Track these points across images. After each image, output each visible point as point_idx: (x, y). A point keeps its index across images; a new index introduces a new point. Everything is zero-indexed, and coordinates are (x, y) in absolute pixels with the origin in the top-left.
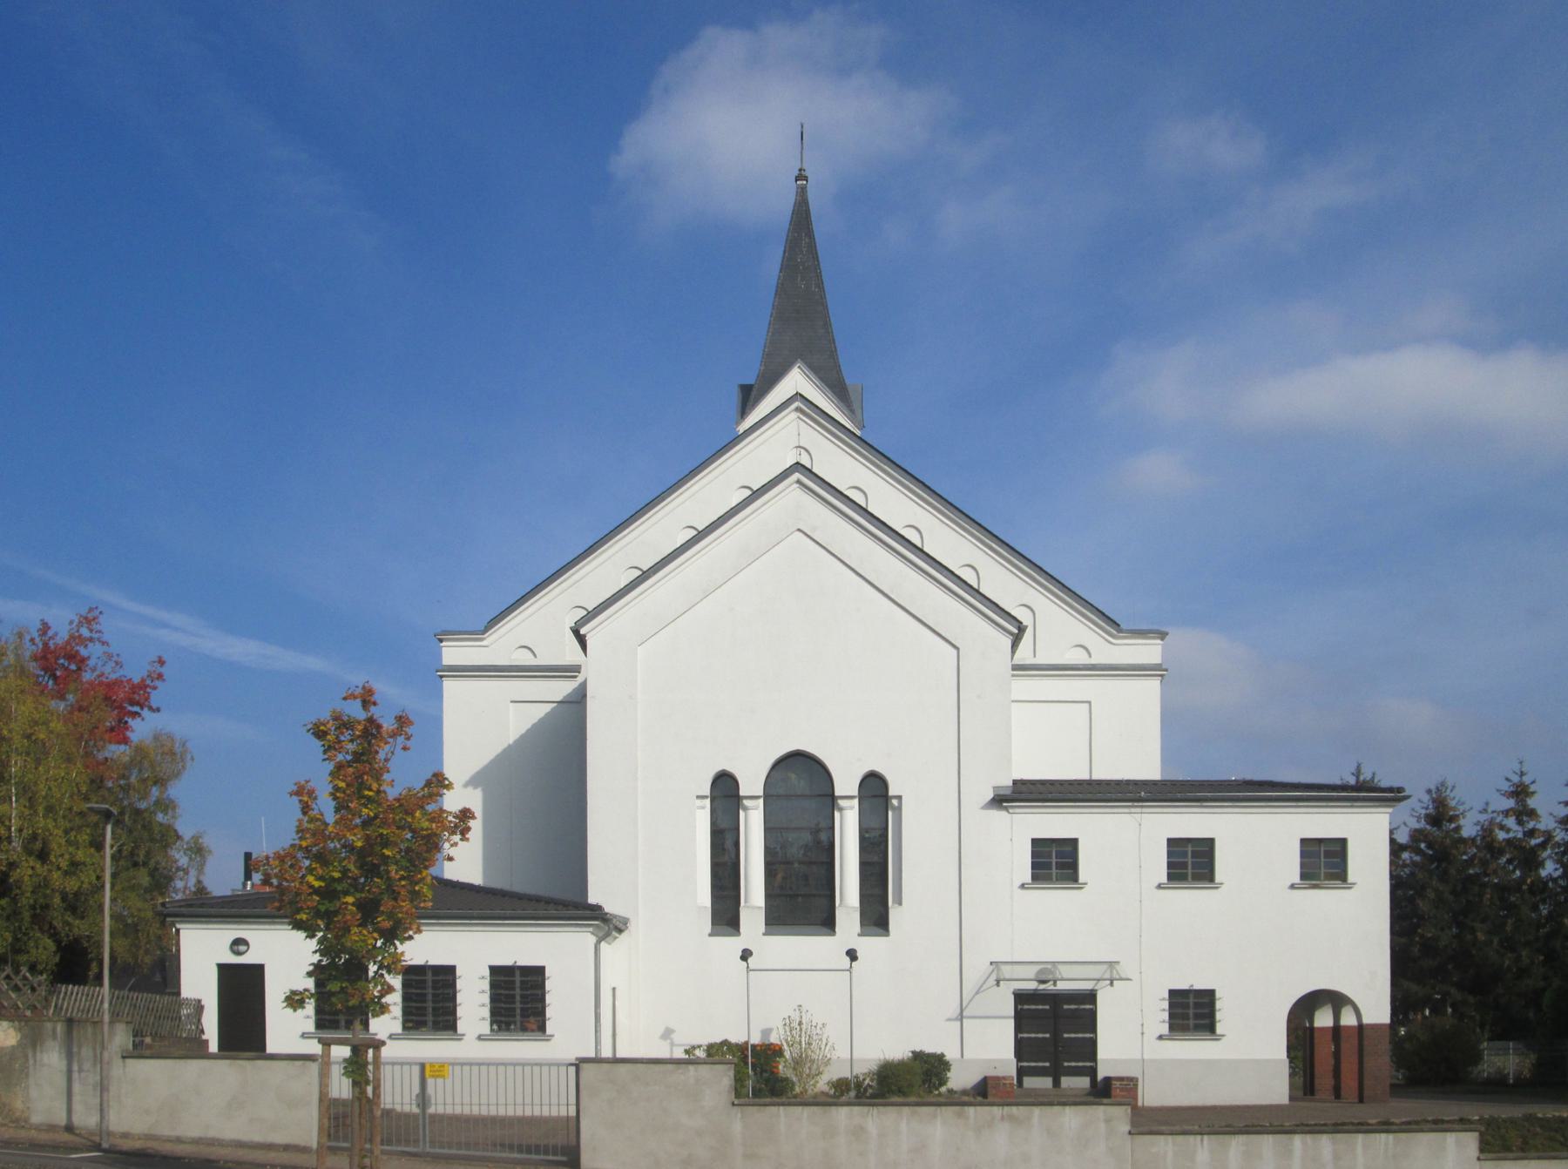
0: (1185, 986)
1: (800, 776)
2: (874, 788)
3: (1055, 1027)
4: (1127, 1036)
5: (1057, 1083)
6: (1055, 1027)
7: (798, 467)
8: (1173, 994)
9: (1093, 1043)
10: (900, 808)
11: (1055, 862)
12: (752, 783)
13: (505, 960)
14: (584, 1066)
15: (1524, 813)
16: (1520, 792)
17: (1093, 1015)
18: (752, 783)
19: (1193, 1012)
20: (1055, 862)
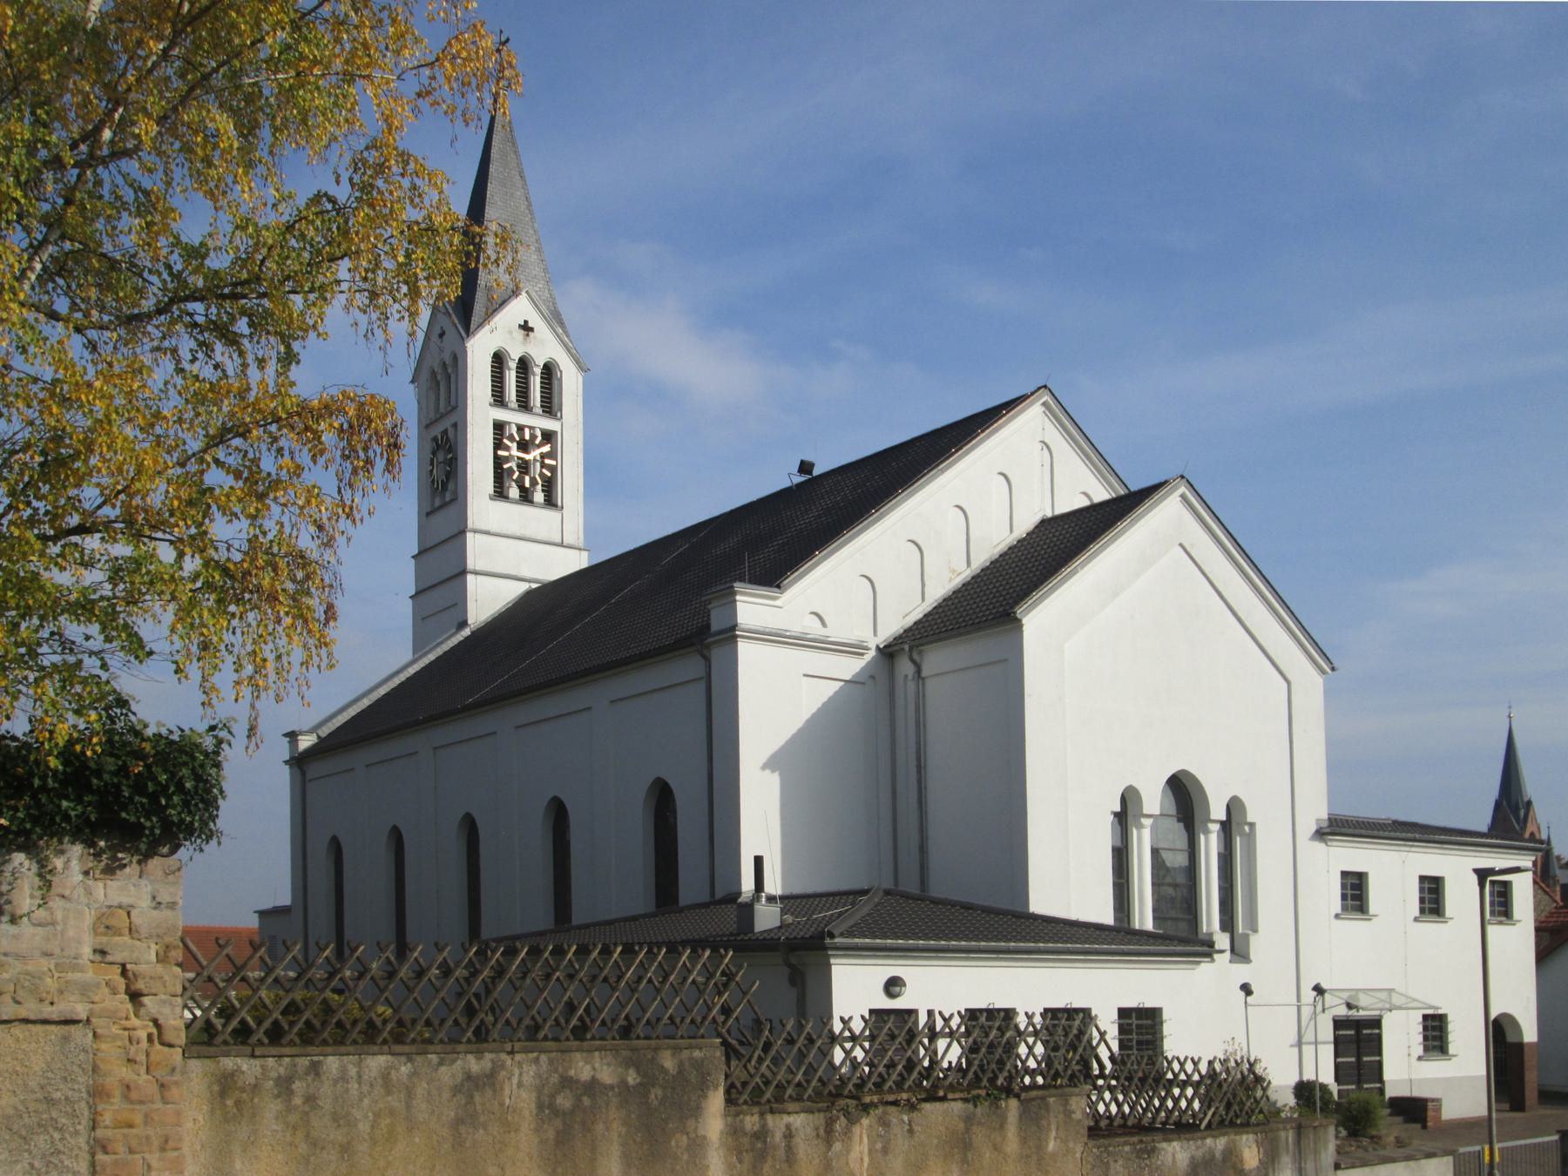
17: (1379, 1037)
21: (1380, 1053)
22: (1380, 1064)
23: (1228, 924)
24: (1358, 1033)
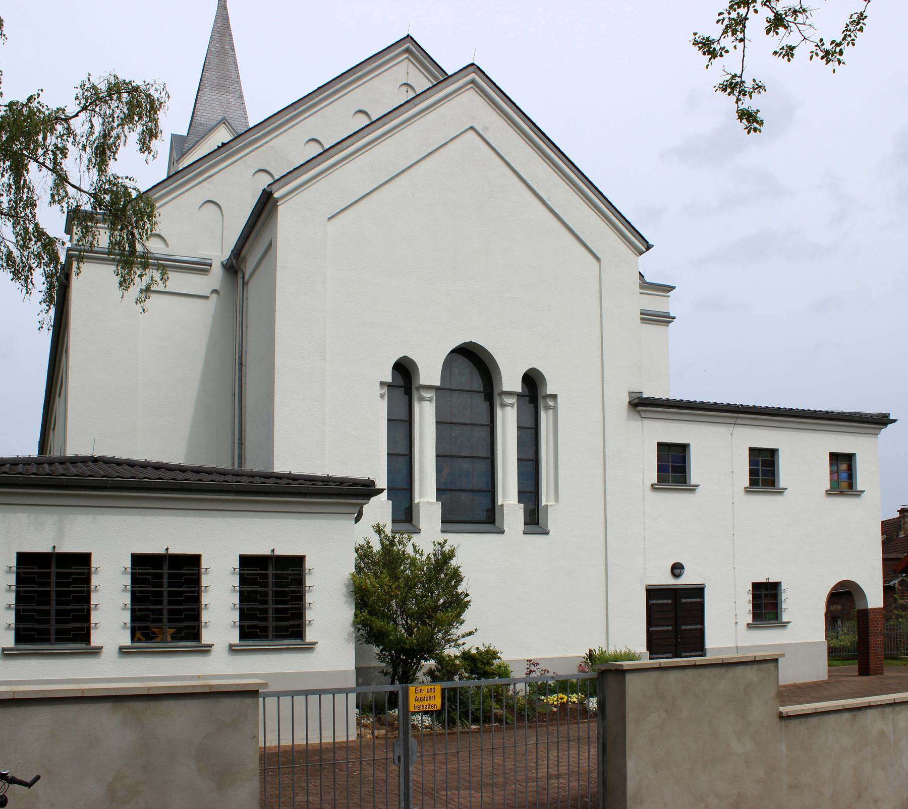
0: (763, 580)
1: (472, 360)
2: (532, 381)
3: (675, 614)
4: (727, 628)
5: (676, 630)
6: (675, 614)
7: (472, 128)
8: (756, 586)
9: (702, 633)
10: (555, 408)
11: (673, 465)
12: (430, 373)
13: (153, 547)
14: (468, 106)
15: (756, 113)
16: (758, 111)
17: (701, 605)
18: (430, 373)
19: (766, 601)
20: (673, 465)
21: (702, 622)
22: (702, 632)
23: (530, 493)
24: (676, 602)
